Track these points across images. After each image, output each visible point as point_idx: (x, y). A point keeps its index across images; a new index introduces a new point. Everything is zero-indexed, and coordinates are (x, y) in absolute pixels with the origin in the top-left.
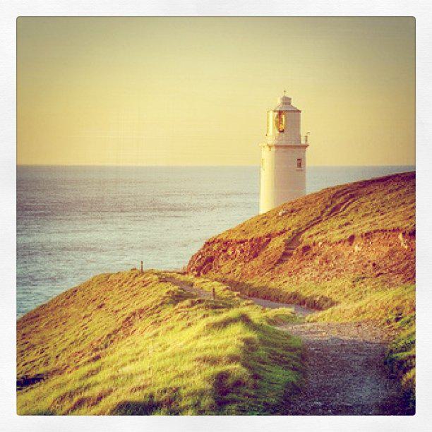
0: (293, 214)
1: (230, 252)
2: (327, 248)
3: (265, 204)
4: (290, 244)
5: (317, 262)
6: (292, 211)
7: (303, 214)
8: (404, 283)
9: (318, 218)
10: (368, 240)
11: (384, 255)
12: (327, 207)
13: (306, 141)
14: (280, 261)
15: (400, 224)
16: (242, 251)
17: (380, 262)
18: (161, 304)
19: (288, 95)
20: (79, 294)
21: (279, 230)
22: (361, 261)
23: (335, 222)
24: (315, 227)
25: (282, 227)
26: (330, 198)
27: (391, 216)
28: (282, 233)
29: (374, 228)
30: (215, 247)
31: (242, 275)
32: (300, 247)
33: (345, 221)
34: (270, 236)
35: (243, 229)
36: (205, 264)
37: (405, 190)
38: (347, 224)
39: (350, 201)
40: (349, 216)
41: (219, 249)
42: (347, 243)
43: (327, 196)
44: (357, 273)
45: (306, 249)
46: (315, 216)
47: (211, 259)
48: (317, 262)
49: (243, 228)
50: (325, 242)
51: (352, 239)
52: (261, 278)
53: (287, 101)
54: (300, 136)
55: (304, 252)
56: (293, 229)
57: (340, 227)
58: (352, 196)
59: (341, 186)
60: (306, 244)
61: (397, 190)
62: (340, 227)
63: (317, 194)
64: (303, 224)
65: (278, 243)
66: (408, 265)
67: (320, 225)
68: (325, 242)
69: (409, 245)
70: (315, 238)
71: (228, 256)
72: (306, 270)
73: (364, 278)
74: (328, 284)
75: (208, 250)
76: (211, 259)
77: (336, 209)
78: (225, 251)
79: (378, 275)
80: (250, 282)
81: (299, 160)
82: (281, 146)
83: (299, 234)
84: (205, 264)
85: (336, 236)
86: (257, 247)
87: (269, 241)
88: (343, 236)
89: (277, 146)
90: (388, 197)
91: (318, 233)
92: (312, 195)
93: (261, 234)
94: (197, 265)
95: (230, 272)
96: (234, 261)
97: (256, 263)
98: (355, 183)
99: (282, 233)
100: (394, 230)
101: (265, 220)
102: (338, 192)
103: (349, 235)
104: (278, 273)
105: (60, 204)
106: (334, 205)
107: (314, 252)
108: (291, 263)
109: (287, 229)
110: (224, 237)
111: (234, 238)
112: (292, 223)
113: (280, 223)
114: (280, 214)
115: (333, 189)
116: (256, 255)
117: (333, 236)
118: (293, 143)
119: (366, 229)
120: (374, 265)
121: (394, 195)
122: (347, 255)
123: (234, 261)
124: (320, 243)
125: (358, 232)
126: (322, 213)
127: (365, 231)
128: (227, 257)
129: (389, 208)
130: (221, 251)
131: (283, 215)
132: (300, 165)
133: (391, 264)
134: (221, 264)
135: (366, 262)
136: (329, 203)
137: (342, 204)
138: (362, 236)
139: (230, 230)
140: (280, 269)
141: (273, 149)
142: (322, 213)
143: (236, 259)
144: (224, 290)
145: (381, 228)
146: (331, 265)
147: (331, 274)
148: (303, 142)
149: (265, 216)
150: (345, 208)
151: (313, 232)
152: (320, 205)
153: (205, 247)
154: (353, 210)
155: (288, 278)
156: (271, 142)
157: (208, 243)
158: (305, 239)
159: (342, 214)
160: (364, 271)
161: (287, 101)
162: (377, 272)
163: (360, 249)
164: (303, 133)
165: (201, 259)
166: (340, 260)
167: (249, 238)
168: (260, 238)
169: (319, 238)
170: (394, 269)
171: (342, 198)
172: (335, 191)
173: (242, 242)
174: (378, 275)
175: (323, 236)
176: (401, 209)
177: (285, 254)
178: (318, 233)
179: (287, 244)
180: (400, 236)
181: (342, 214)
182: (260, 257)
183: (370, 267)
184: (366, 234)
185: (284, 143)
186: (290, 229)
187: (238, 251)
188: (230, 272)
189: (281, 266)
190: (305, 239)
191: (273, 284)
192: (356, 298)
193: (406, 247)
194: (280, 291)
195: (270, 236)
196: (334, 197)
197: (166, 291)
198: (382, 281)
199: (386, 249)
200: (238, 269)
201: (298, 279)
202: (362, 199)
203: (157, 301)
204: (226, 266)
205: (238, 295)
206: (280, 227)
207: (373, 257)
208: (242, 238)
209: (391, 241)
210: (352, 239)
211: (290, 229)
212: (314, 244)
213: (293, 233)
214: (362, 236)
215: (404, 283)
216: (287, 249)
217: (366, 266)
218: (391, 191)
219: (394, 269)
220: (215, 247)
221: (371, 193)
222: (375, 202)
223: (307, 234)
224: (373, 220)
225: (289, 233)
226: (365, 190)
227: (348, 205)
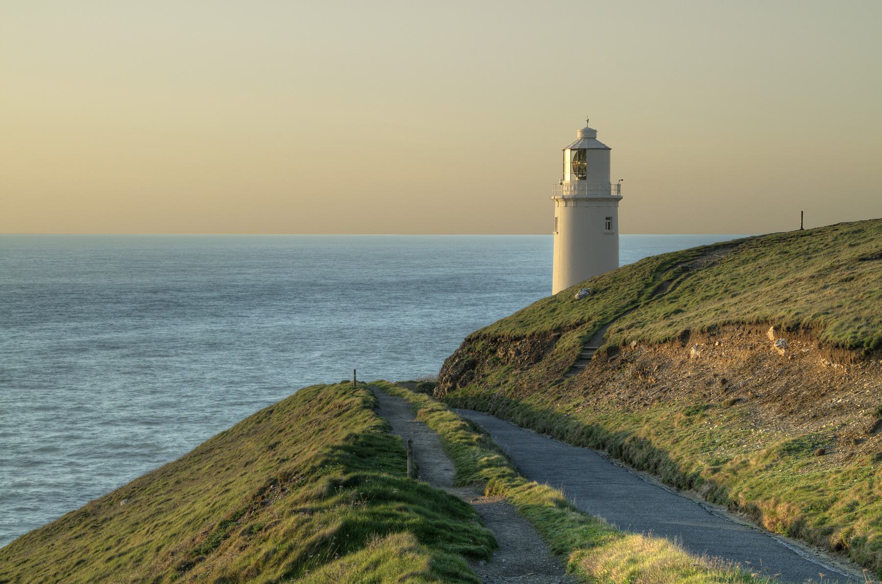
0: (596, 296)
1: (500, 354)
2: (645, 350)
3: (557, 286)
4: (587, 343)
5: (628, 373)
6: (595, 292)
7: (611, 297)
8: (782, 419)
9: (633, 302)
10: (712, 339)
11: (741, 364)
12: (647, 286)
13: (619, 191)
14: (574, 369)
15: (767, 312)
16: (518, 353)
17: (735, 376)
18: (322, 466)
19: (592, 126)
20: (275, 416)
21: (573, 321)
22: (700, 376)
23: (660, 309)
24: (629, 316)
25: (579, 316)
26: (651, 272)
27: (750, 299)
28: (578, 325)
29: (723, 319)
30: (479, 346)
31: (516, 390)
32: (603, 348)
33: (674, 306)
34: (560, 331)
35: (521, 319)
36: (463, 372)
37: (767, 259)
38: (677, 312)
39: (683, 276)
40: (681, 299)
41: (484, 349)
42: (677, 344)
43: (648, 268)
44: (695, 395)
45: (613, 351)
46: (628, 300)
47: (473, 364)
48: (628, 373)
49: (521, 318)
50: (641, 342)
51: (685, 336)
52: (542, 397)
53: (589, 134)
54: (609, 184)
55: (609, 355)
56: (595, 319)
57: (667, 316)
58: (685, 270)
59: (669, 254)
60: (612, 344)
61: (754, 260)
62: (667, 316)
63: (632, 267)
64: (611, 311)
65: (570, 340)
66: (787, 387)
67: (636, 313)
68: (641, 342)
69: (787, 348)
70: (626, 333)
71: (498, 359)
72: (610, 386)
73: (707, 407)
74: (646, 413)
75: (469, 350)
76: (473, 364)
77: (661, 288)
78: (493, 352)
79: (733, 402)
80: (526, 401)
81: (608, 218)
82: (582, 199)
83: (604, 325)
84: (463, 372)
85: (660, 330)
86: (540, 346)
87: (559, 336)
88: (669, 332)
89: (576, 199)
90: (741, 270)
91: (632, 326)
92: (625, 267)
93: (547, 326)
94: (452, 372)
95: (499, 385)
96: (505, 368)
97: (538, 371)
98: (688, 251)
99: (578, 325)
100: (758, 322)
101: (553, 306)
102: (663, 264)
103: (681, 329)
104: (569, 389)
105: (749, 279)
106: (658, 283)
107: (624, 357)
108: (588, 371)
109: (586, 318)
110: (492, 331)
111: (507, 332)
112: (594, 310)
113: (575, 310)
114: (576, 296)
115: (657, 258)
116: (539, 359)
117: (655, 330)
118: (600, 196)
119: (709, 320)
120: (724, 381)
121: (750, 267)
122: (677, 363)
123: (505, 368)
124: (634, 343)
125: (696, 325)
126: (640, 294)
127: (708, 324)
128: (496, 362)
129: (744, 287)
130: (487, 352)
131: (581, 297)
132: (609, 226)
133: (754, 383)
134: (486, 372)
135: (710, 376)
136: (650, 280)
137: (671, 281)
138: (702, 332)
139: (502, 321)
140: (571, 382)
141: (571, 204)
142: (640, 294)
143: (509, 365)
144: (457, 430)
145: (734, 318)
146: (651, 380)
147: (651, 394)
148: (614, 193)
149: (555, 299)
150: (674, 289)
151: (624, 324)
152: (636, 283)
153: (463, 346)
154: (687, 291)
155: (581, 399)
156: (567, 193)
157: (469, 340)
158: (612, 335)
159: (670, 295)
160: (706, 393)
161: (589, 134)
162: (732, 398)
163: (698, 353)
164: (614, 180)
165: (457, 364)
166: (666, 372)
167: (529, 333)
168: (545, 332)
169: (633, 334)
170: (761, 392)
171: (670, 272)
172: (660, 262)
173: (517, 339)
174: (733, 402)
175: (639, 332)
176: (763, 288)
177: (581, 359)
178: (632, 326)
179: (585, 343)
180: (770, 334)
181: (670, 295)
182: (543, 364)
183: (717, 386)
184: (710, 329)
185: (586, 194)
186: (589, 319)
187: (512, 352)
188: (499, 385)
189: (573, 376)
190: (612, 335)
191: (558, 407)
192: (695, 447)
193: (782, 352)
194: (568, 419)
195: (560, 331)
196: (657, 271)
197: (345, 433)
198: (742, 415)
199: (744, 355)
200: (511, 380)
201: (598, 400)
202: (701, 274)
203: (316, 457)
204: (493, 376)
205: (478, 440)
206: (575, 316)
207: (720, 367)
208: (519, 332)
209: (754, 341)
210: (685, 336)
211: (589, 319)
212: (625, 344)
213: (594, 326)
214: (702, 332)
215: (782, 419)
216: (584, 350)
217: (710, 384)
218: (745, 262)
219: (761, 392)
220: (479, 346)
221: (714, 264)
222: (721, 277)
223: (615, 326)
224: (719, 305)
225: (589, 325)
226: (705, 260)
227: (679, 282)
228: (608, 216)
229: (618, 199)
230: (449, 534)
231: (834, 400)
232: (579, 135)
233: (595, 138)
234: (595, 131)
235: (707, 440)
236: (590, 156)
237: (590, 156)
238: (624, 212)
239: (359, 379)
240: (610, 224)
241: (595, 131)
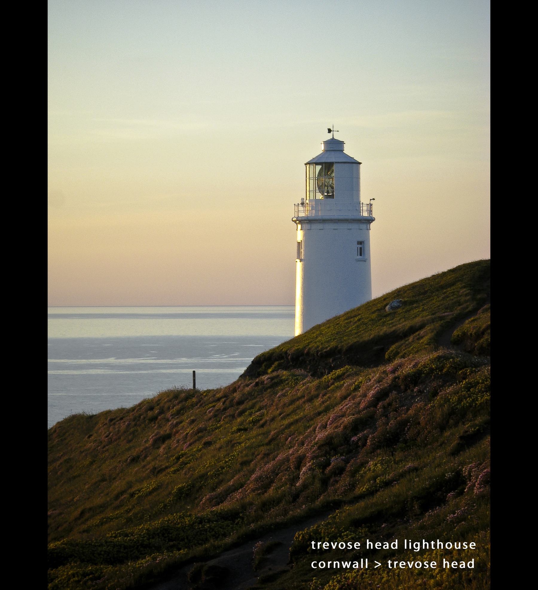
13: (370, 211)
53: (334, 146)
81: (360, 243)
148: (365, 214)
161: (334, 146)
164: (364, 199)
228: (360, 240)
229: (370, 220)
230: (126, 496)
231: (425, 460)
232: (322, 147)
233: (342, 150)
234: (342, 143)
235: (186, 540)
236: (334, 168)
237: (334, 168)
238: (376, 234)
239: (202, 386)
240: (362, 248)
241: (342, 143)
